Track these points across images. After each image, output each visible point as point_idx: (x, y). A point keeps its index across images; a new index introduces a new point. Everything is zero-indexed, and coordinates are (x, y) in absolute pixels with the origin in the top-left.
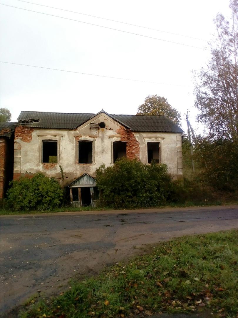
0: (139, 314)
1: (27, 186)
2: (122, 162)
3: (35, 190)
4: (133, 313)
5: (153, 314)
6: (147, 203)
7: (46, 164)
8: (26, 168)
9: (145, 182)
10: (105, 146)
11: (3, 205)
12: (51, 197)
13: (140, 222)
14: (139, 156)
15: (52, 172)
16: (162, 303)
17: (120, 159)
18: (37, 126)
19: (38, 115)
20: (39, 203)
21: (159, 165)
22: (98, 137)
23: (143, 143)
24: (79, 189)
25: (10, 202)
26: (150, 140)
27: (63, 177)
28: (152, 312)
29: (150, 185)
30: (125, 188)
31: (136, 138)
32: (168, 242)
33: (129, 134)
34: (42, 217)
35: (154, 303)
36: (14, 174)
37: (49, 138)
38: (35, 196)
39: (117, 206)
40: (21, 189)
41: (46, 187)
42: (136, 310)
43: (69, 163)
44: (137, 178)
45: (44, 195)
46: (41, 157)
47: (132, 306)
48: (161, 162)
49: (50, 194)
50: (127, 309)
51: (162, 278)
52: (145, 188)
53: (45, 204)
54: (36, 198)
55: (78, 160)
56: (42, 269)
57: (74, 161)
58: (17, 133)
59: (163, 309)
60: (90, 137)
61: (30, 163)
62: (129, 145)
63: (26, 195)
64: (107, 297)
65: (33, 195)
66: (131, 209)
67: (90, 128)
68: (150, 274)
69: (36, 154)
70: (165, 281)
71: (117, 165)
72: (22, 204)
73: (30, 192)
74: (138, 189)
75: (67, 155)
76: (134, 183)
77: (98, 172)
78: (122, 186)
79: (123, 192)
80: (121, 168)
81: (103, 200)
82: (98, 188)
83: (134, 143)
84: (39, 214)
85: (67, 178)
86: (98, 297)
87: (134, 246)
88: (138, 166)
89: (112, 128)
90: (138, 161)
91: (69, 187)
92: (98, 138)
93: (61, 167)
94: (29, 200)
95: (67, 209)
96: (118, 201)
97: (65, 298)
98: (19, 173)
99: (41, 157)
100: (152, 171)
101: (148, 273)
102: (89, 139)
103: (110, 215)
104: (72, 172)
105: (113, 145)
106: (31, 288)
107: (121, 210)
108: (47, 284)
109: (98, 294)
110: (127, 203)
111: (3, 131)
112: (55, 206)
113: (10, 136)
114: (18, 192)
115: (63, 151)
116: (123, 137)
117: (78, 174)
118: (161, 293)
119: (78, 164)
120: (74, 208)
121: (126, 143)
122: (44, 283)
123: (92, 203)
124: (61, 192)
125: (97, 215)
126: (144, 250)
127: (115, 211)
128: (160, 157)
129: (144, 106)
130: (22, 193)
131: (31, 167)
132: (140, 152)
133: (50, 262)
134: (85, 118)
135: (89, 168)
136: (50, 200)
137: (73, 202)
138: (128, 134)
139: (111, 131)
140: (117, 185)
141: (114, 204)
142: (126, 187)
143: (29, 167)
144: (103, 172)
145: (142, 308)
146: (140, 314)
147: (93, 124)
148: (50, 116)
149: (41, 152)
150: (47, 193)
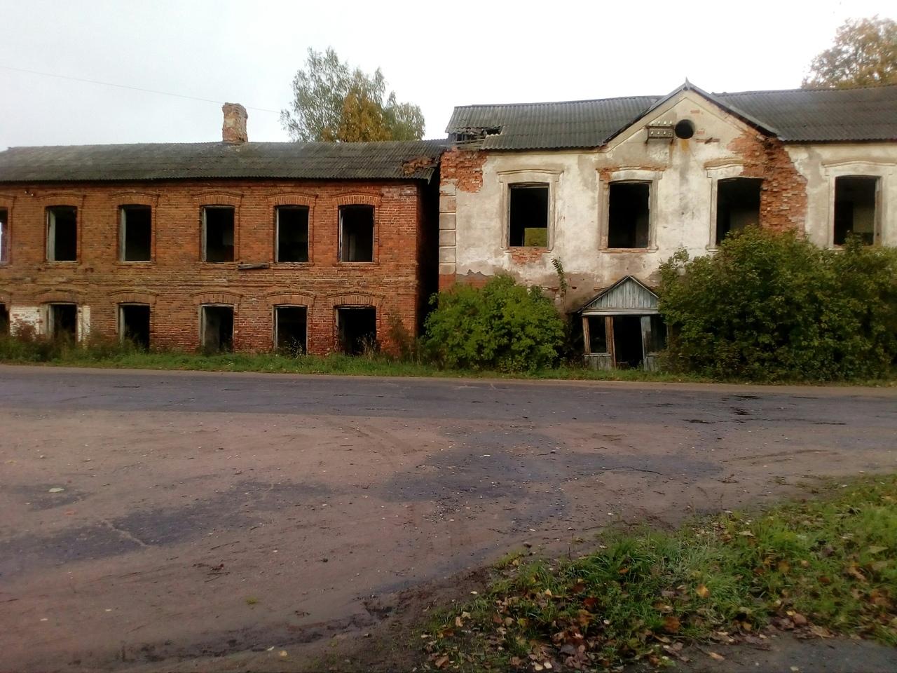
0: (792, 629)
1: (473, 306)
2: (745, 241)
3: (491, 317)
4: (777, 625)
5: (833, 636)
6: (824, 369)
7: (519, 250)
8: (468, 262)
9: (821, 303)
10: (690, 195)
11: (418, 352)
12: (533, 338)
13: (800, 420)
14: (804, 221)
15: (534, 273)
16: (862, 617)
17: (737, 232)
18: (495, 145)
19: (499, 115)
20: (502, 351)
21: (874, 252)
22: (670, 166)
23: (820, 180)
24: (608, 320)
25: (433, 346)
26: (846, 170)
27: (563, 285)
28: (832, 631)
29: (837, 312)
30: (751, 320)
31: (796, 164)
32: (888, 476)
33: (772, 154)
34: (511, 386)
35: (837, 613)
36: (440, 278)
37: (525, 178)
38: (491, 333)
39: (724, 372)
40: (458, 314)
41: (519, 311)
42: (786, 621)
43: (580, 248)
44: (794, 291)
45: (516, 333)
46: (506, 231)
47: (774, 608)
48: (879, 243)
49: (529, 329)
50: (759, 614)
51: (865, 560)
52: (820, 322)
53: (517, 356)
54: (495, 338)
55: (605, 239)
56: (527, 500)
57: (594, 240)
58: (445, 169)
59: (864, 630)
60: (644, 168)
61: (479, 246)
62: (770, 188)
63: (470, 331)
64: (704, 580)
65: (487, 332)
66: (769, 384)
67: (646, 143)
68: (829, 546)
69: (493, 224)
70: (873, 567)
71: (728, 252)
72: (461, 353)
73: (479, 323)
74: (795, 325)
75: (576, 225)
76: (781, 307)
77: (667, 272)
78: (742, 315)
79: (744, 332)
80: (742, 261)
81: (679, 352)
82: (664, 318)
83: (789, 180)
84: (503, 380)
85: (575, 288)
86: (678, 576)
87: (777, 477)
88: (799, 254)
89: (715, 137)
90: (799, 237)
91: (581, 313)
92: (668, 171)
93: (557, 264)
94: (478, 344)
95: (574, 372)
96: (727, 357)
97: (594, 565)
98: (452, 273)
99: (505, 232)
100: (846, 271)
101: (822, 543)
102: (641, 175)
103: (702, 394)
104: (589, 272)
105: (716, 189)
106: (508, 536)
107: (735, 383)
108: (546, 534)
109: (677, 570)
110: (757, 364)
111: (412, 164)
112: (543, 361)
113: (429, 178)
114: (453, 320)
115: (565, 214)
116: (753, 162)
117: (607, 277)
118: (860, 593)
119: (605, 249)
120: (593, 371)
121: (760, 181)
122: (538, 530)
123: (645, 361)
124: (557, 326)
125: (660, 392)
126: (810, 490)
127: (716, 385)
128: (879, 224)
129: (831, 56)
130: (461, 324)
131: (480, 259)
132: (809, 210)
133: (545, 487)
134: (630, 110)
135: (637, 260)
136: (531, 347)
137: (592, 355)
138: (768, 154)
139: (712, 146)
140: (726, 312)
141: (715, 366)
142: (755, 317)
143: (477, 259)
144: (682, 271)
145: (801, 618)
146: (795, 631)
147: (656, 127)
148: (529, 114)
149: (506, 216)
150: (523, 327)
